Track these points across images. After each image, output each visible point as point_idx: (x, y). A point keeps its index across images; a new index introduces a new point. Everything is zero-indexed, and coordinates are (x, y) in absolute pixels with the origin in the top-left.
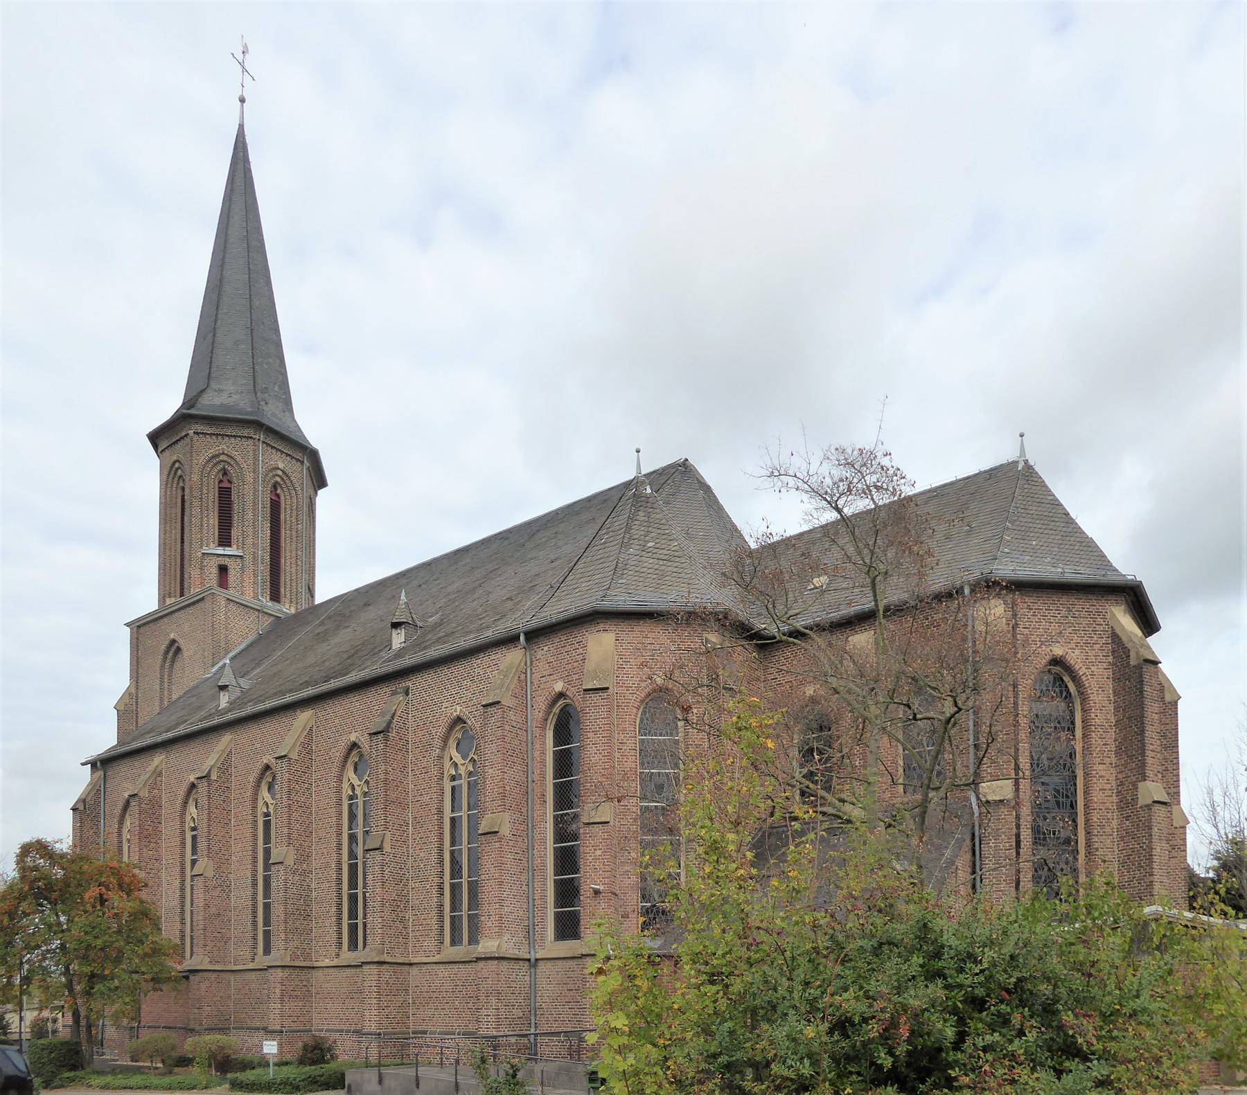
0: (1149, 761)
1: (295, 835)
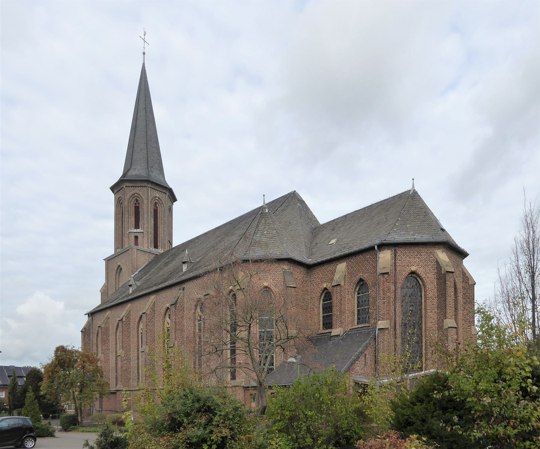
0: (448, 311)
1: (149, 341)
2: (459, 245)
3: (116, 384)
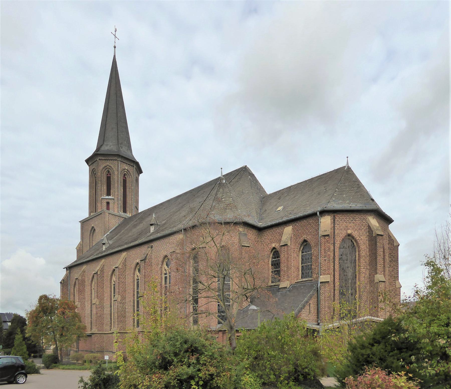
0: (378, 268)
1: (121, 292)
2: (386, 213)
3: (91, 329)
